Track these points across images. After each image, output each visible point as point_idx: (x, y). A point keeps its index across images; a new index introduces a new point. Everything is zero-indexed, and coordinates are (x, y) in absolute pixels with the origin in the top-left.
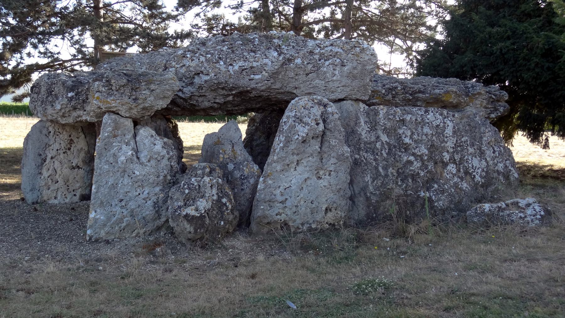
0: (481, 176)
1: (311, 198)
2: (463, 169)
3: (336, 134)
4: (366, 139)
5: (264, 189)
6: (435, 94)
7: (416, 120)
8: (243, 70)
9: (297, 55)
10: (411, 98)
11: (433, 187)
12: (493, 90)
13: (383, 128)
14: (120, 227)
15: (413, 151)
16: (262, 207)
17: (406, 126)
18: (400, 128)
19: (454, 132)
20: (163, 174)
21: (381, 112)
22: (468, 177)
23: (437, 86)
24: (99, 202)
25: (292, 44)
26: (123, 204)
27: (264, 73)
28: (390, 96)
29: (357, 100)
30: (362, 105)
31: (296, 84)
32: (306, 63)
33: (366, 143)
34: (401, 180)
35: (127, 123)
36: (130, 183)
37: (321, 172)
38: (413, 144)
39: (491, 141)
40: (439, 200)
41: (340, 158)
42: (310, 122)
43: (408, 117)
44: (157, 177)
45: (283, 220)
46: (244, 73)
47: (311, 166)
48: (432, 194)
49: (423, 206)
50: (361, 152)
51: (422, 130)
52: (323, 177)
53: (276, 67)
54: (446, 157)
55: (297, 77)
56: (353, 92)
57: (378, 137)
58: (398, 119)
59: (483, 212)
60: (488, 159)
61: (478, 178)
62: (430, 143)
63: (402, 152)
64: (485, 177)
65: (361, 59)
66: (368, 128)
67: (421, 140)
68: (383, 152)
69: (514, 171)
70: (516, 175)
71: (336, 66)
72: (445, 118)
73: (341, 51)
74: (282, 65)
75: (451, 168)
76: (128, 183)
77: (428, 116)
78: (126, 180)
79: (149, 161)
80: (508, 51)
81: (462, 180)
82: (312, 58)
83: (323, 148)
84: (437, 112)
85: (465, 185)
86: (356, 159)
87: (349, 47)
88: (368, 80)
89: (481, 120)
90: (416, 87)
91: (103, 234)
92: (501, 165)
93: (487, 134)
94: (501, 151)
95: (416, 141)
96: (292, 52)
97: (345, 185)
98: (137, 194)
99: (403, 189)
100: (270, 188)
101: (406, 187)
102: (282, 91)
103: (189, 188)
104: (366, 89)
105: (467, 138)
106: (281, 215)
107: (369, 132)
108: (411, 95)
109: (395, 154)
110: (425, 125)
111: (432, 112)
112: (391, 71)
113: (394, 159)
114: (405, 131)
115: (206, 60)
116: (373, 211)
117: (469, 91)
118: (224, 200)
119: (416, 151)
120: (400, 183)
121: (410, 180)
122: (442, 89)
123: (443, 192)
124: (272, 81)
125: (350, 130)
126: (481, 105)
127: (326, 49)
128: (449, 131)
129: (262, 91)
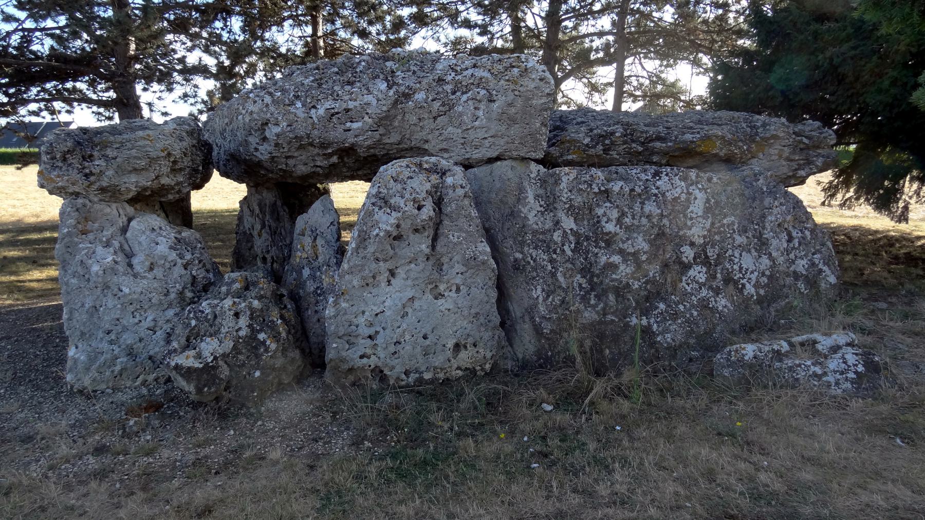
0: (757, 286)
1: (424, 331)
2: (722, 273)
3: (462, 222)
4: (535, 226)
5: (335, 317)
6: (684, 142)
7: (632, 190)
8: (333, 115)
9: (418, 85)
10: (640, 149)
11: (657, 308)
12: (807, 129)
13: (567, 206)
14: (113, 371)
15: (621, 245)
16: (334, 345)
17: (610, 202)
18: (598, 205)
19: (708, 210)
20: (175, 290)
21: (564, 179)
22: (731, 287)
23: (691, 128)
24: (78, 333)
25: (412, 68)
26: (113, 337)
27: (366, 118)
28: (600, 147)
29: (524, 159)
30: (534, 167)
31: (423, 135)
32: (430, 98)
33: (535, 232)
34: (595, 296)
35: (108, 210)
36: (119, 306)
37: (442, 287)
38: (622, 234)
39: (785, 221)
40: (666, 330)
41: (471, 263)
42: (402, 205)
43: (616, 186)
44: (166, 295)
45: (373, 367)
46: (334, 119)
47: (416, 278)
48: (652, 320)
49: (633, 338)
50: (526, 249)
51: (642, 208)
52: (446, 294)
53: (385, 108)
54: (688, 253)
55: (421, 124)
56: (512, 146)
57: (557, 223)
58: (596, 190)
59: (741, 360)
60: (774, 254)
61: (750, 289)
62: (656, 231)
63: (600, 248)
64: (766, 285)
65: (521, 89)
66: (541, 206)
67: (638, 227)
68: (566, 248)
69: (828, 272)
70: (832, 279)
71: (480, 101)
72: (691, 185)
73: (489, 75)
74: (396, 102)
75: (698, 273)
76: (115, 306)
77: (659, 183)
78: (111, 302)
79: (151, 269)
80: (844, 60)
81: (718, 294)
82: (440, 90)
83: (438, 248)
84: (676, 175)
85: (722, 303)
86: (516, 260)
87: (501, 67)
88: (538, 125)
89: (768, 186)
90: (652, 131)
91: (87, 382)
92: (804, 262)
93: (775, 211)
94: (803, 238)
95: (628, 228)
96: (411, 82)
97: (488, 307)
98: (136, 320)
99: (597, 312)
100: (345, 314)
101: (604, 309)
102: (406, 146)
103: (197, 318)
104: (537, 141)
105: (733, 218)
106: (369, 357)
107: (542, 213)
108: (643, 144)
109: (588, 252)
110: (648, 199)
111: (667, 175)
112: (692, 100)
113: (585, 259)
114: (608, 212)
115: (273, 101)
116: (547, 346)
117: (757, 134)
118: (262, 336)
119: (626, 246)
120: (592, 302)
121: (612, 297)
122: (698, 133)
123: (675, 316)
124: (382, 130)
125: (507, 211)
126: (780, 157)
127: (465, 73)
128: (697, 207)
129: (369, 147)
